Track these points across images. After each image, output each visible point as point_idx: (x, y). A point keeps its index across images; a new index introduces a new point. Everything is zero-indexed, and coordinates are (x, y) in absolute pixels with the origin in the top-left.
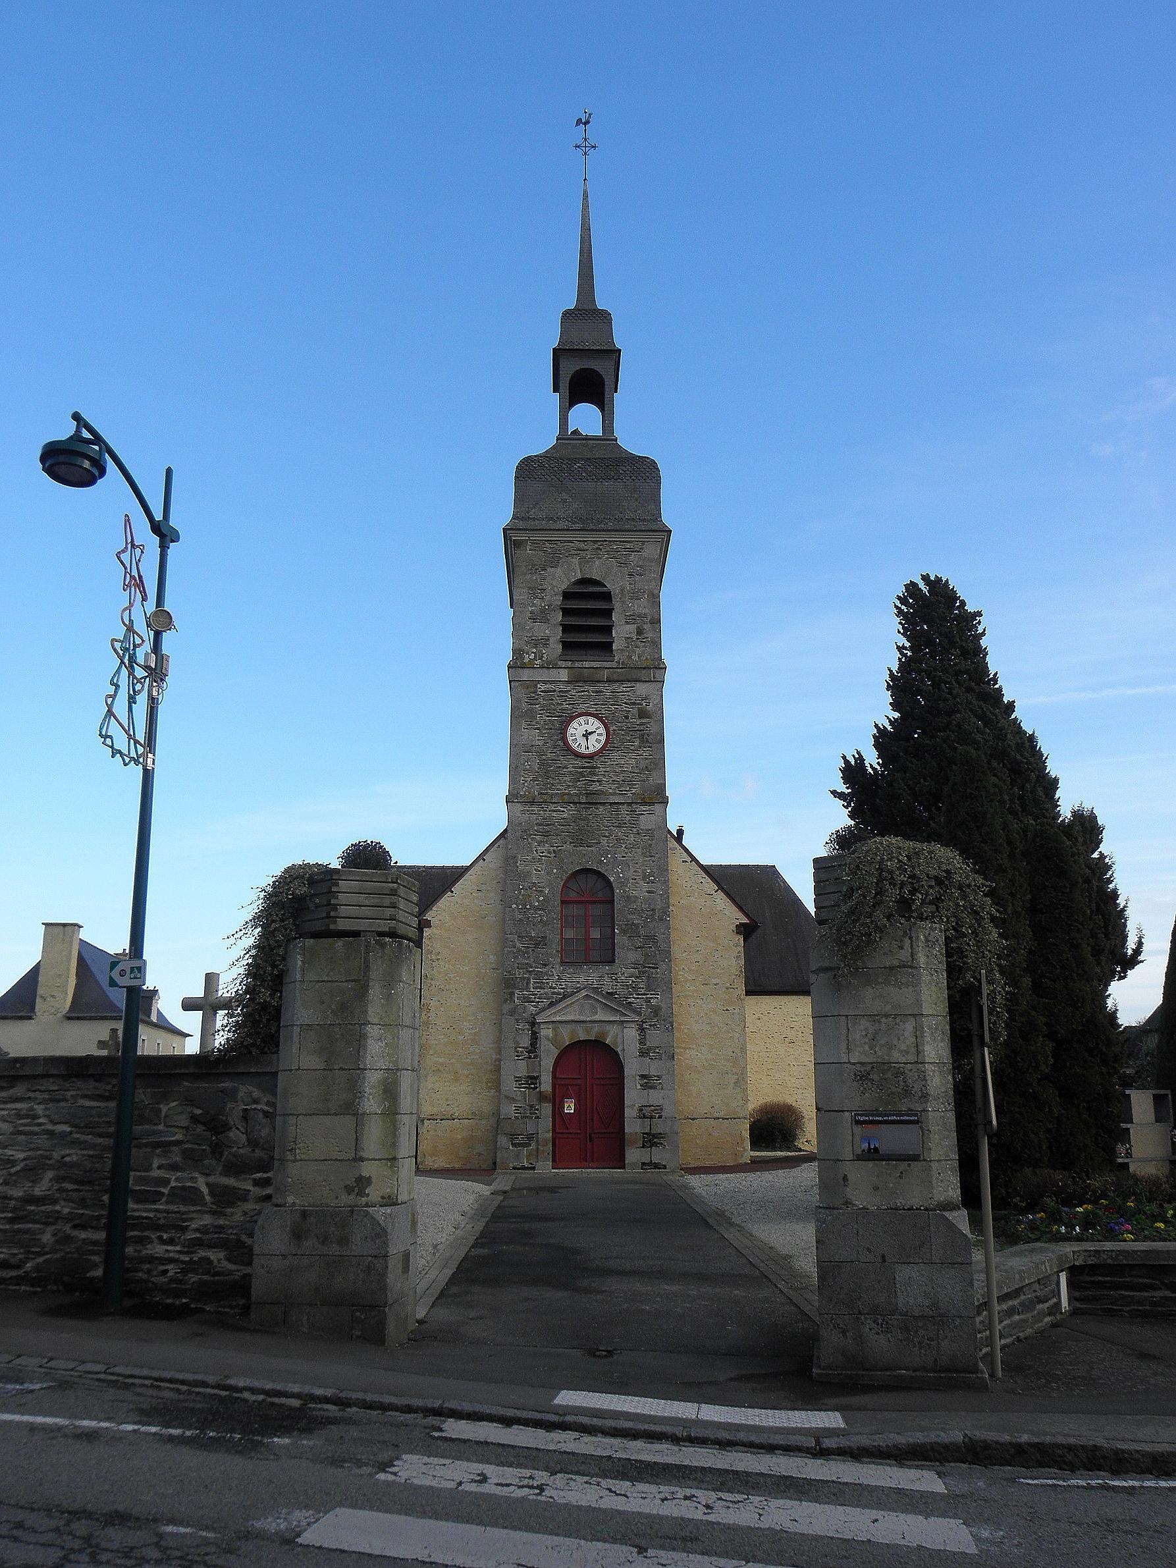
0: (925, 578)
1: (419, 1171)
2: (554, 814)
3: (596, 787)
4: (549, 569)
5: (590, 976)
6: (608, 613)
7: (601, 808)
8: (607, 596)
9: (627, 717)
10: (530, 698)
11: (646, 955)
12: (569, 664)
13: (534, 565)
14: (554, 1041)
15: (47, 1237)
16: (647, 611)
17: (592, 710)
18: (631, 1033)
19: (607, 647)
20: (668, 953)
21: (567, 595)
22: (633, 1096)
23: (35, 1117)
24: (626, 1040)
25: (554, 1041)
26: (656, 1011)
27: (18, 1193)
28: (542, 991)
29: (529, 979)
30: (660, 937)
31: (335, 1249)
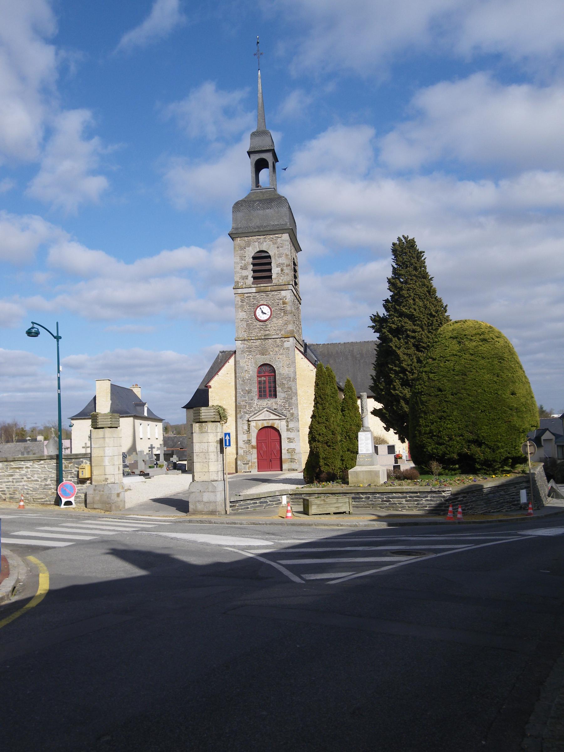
0: (403, 236)
1: (237, 472)
2: (253, 344)
3: (267, 332)
4: (247, 248)
5: (265, 402)
6: (270, 264)
7: (270, 340)
8: (269, 257)
9: (278, 305)
10: (242, 300)
11: (289, 395)
12: (256, 286)
13: (241, 247)
14: (256, 427)
15: (50, 493)
16: (284, 261)
17: (265, 303)
18: (284, 423)
19: (270, 277)
20: (296, 394)
21: (254, 258)
22: (285, 445)
23: (45, 468)
24: (281, 425)
25: (256, 427)
26: (292, 414)
27: (43, 484)
28: (251, 409)
29: (246, 405)
30: (293, 388)
31: (102, 493)
